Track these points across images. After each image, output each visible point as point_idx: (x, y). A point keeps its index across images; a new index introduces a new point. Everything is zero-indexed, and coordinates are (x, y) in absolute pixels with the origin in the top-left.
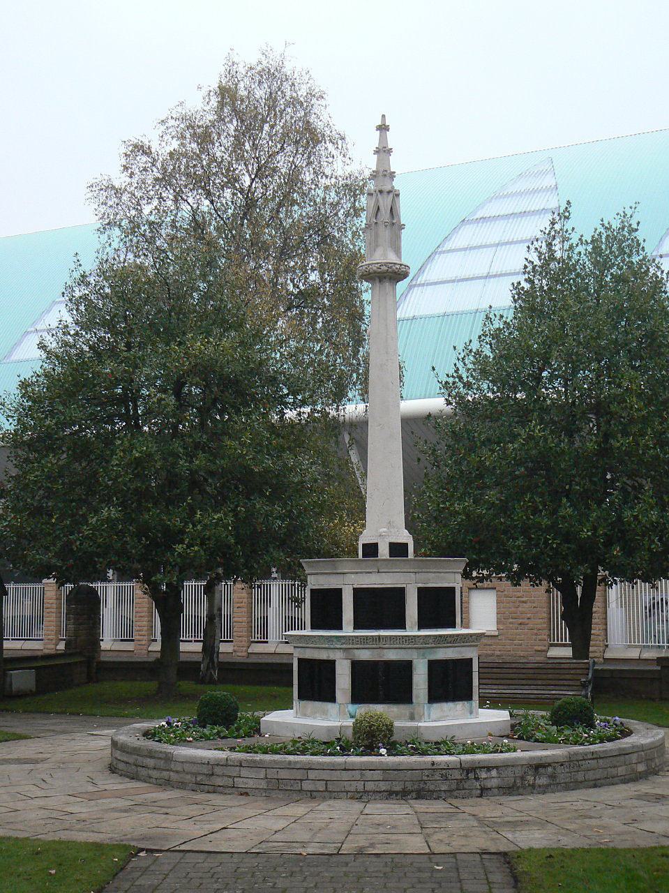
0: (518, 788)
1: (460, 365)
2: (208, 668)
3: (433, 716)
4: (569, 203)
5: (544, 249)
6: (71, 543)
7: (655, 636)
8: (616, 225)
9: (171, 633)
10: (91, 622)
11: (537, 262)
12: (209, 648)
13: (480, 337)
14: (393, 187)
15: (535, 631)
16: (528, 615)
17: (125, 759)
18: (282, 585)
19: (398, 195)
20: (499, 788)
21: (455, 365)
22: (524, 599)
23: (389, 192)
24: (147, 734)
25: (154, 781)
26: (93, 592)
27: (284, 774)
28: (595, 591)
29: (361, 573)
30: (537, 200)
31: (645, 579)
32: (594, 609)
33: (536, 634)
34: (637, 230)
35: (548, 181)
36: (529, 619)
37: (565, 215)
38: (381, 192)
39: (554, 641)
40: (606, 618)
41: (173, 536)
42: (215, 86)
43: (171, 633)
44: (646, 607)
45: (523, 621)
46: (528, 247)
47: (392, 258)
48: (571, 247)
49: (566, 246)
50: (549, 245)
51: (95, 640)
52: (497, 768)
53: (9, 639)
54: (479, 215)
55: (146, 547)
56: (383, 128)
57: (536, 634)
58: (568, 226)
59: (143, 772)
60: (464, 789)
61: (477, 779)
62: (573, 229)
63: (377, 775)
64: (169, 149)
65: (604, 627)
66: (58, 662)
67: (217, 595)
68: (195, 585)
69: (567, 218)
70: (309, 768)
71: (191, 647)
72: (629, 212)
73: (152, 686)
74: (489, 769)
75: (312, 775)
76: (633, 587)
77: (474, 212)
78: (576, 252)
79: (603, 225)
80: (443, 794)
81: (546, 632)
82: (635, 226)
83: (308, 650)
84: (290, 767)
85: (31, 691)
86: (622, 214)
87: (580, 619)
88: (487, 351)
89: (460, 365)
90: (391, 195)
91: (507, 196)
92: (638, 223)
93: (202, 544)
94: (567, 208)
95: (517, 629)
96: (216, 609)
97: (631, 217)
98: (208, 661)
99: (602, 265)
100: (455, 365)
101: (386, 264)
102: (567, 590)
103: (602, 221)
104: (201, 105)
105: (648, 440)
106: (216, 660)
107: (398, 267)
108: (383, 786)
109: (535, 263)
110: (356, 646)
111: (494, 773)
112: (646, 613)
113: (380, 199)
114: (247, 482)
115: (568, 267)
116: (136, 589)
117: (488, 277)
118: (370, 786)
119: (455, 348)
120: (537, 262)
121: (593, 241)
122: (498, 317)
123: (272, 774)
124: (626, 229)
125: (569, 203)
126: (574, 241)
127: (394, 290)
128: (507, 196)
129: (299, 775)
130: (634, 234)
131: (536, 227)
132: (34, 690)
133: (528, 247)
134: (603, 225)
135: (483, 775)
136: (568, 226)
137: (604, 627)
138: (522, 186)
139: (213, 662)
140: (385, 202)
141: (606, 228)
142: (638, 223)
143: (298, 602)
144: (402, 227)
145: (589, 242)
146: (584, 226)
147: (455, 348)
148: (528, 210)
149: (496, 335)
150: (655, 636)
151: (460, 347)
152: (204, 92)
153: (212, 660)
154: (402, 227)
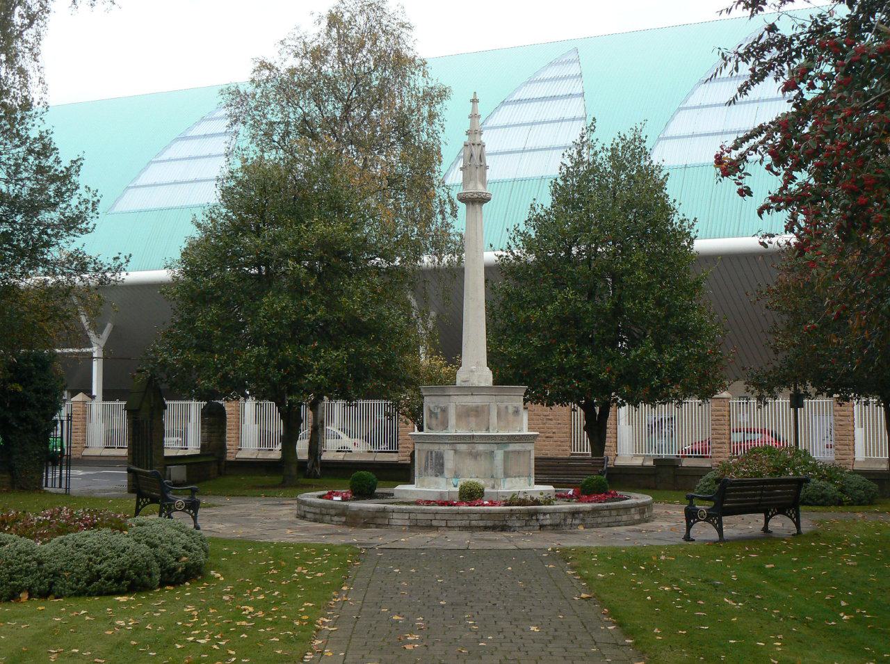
0: (562, 525)
1: (512, 243)
2: (313, 466)
3: (506, 486)
4: (594, 119)
5: (575, 156)
6: (227, 374)
7: (655, 448)
8: (629, 137)
9: (289, 439)
10: (221, 431)
11: (569, 164)
12: (315, 448)
13: (526, 222)
14: (481, 141)
15: (559, 443)
16: (554, 431)
17: (313, 511)
18: (374, 404)
19: (484, 146)
20: (550, 525)
21: (508, 243)
22: (550, 417)
23: (479, 145)
24: (320, 497)
25: (335, 523)
26: (222, 408)
27: (420, 516)
28: (609, 411)
29: (461, 395)
30: (566, 84)
31: (646, 402)
32: (608, 426)
33: (560, 446)
34: (645, 142)
35: (573, 70)
36: (554, 433)
37: (591, 129)
38: (473, 144)
39: (574, 451)
40: (616, 433)
41: (302, 370)
42: (325, 13)
43: (289, 439)
44: (648, 425)
45: (549, 435)
46: (563, 154)
47: (480, 188)
48: (595, 154)
49: (592, 152)
50: (579, 153)
51: (222, 448)
52: (550, 513)
53: (114, 448)
54: (516, 97)
55: (283, 377)
56: (474, 101)
57: (560, 446)
58: (594, 137)
59: (328, 518)
60: (530, 526)
61: (537, 520)
62: (597, 140)
63: (477, 517)
64: (288, 65)
65: (615, 440)
66: (44, 480)
67: (320, 411)
68: (782, 403)
69: (593, 131)
70: (436, 513)
71: (302, 447)
72: (639, 127)
73: (277, 479)
74: (545, 514)
75: (438, 517)
76: (636, 411)
77: (511, 95)
78: (599, 157)
79: (620, 137)
80: (517, 529)
81: (568, 444)
82: (643, 138)
83: (425, 445)
84: (424, 512)
85: (184, 481)
86: (635, 128)
87: (597, 429)
88: (533, 233)
89: (512, 243)
90: (480, 147)
91: (541, 81)
92: (646, 137)
93: (326, 375)
94: (592, 123)
95: (544, 441)
96: (319, 421)
97: (641, 131)
98: (313, 460)
99: (619, 165)
100: (508, 243)
101: (477, 193)
102: (588, 409)
103: (619, 133)
104: (315, 32)
105: (650, 303)
106: (319, 460)
107: (484, 194)
108: (481, 523)
109: (569, 166)
110: (457, 442)
111: (548, 516)
112: (648, 430)
113: (473, 150)
114: (357, 329)
115: (594, 169)
116: (271, 406)
117: (523, 151)
118: (474, 523)
119: (508, 230)
120: (569, 164)
121: (612, 149)
122: (540, 206)
123: (412, 516)
124: (637, 140)
125: (594, 119)
126: (598, 148)
127: (481, 208)
128: (541, 81)
129: (430, 517)
130: (643, 145)
131: (572, 134)
132: (185, 480)
133: (563, 154)
134: (620, 137)
135: (541, 517)
136: (594, 137)
137: (615, 440)
138: (553, 72)
139: (317, 462)
140: (476, 151)
141: (622, 139)
142: (646, 137)
143: (389, 416)
144: (487, 168)
145: (609, 149)
146: (606, 137)
147: (508, 230)
148: (558, 94)
149: (538, 218)
150: (655, 448)
151: (512, 229)
152: (316, 17)
153: (316, 460)
154: (487, 168)
